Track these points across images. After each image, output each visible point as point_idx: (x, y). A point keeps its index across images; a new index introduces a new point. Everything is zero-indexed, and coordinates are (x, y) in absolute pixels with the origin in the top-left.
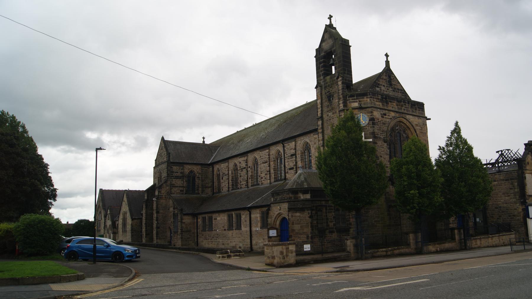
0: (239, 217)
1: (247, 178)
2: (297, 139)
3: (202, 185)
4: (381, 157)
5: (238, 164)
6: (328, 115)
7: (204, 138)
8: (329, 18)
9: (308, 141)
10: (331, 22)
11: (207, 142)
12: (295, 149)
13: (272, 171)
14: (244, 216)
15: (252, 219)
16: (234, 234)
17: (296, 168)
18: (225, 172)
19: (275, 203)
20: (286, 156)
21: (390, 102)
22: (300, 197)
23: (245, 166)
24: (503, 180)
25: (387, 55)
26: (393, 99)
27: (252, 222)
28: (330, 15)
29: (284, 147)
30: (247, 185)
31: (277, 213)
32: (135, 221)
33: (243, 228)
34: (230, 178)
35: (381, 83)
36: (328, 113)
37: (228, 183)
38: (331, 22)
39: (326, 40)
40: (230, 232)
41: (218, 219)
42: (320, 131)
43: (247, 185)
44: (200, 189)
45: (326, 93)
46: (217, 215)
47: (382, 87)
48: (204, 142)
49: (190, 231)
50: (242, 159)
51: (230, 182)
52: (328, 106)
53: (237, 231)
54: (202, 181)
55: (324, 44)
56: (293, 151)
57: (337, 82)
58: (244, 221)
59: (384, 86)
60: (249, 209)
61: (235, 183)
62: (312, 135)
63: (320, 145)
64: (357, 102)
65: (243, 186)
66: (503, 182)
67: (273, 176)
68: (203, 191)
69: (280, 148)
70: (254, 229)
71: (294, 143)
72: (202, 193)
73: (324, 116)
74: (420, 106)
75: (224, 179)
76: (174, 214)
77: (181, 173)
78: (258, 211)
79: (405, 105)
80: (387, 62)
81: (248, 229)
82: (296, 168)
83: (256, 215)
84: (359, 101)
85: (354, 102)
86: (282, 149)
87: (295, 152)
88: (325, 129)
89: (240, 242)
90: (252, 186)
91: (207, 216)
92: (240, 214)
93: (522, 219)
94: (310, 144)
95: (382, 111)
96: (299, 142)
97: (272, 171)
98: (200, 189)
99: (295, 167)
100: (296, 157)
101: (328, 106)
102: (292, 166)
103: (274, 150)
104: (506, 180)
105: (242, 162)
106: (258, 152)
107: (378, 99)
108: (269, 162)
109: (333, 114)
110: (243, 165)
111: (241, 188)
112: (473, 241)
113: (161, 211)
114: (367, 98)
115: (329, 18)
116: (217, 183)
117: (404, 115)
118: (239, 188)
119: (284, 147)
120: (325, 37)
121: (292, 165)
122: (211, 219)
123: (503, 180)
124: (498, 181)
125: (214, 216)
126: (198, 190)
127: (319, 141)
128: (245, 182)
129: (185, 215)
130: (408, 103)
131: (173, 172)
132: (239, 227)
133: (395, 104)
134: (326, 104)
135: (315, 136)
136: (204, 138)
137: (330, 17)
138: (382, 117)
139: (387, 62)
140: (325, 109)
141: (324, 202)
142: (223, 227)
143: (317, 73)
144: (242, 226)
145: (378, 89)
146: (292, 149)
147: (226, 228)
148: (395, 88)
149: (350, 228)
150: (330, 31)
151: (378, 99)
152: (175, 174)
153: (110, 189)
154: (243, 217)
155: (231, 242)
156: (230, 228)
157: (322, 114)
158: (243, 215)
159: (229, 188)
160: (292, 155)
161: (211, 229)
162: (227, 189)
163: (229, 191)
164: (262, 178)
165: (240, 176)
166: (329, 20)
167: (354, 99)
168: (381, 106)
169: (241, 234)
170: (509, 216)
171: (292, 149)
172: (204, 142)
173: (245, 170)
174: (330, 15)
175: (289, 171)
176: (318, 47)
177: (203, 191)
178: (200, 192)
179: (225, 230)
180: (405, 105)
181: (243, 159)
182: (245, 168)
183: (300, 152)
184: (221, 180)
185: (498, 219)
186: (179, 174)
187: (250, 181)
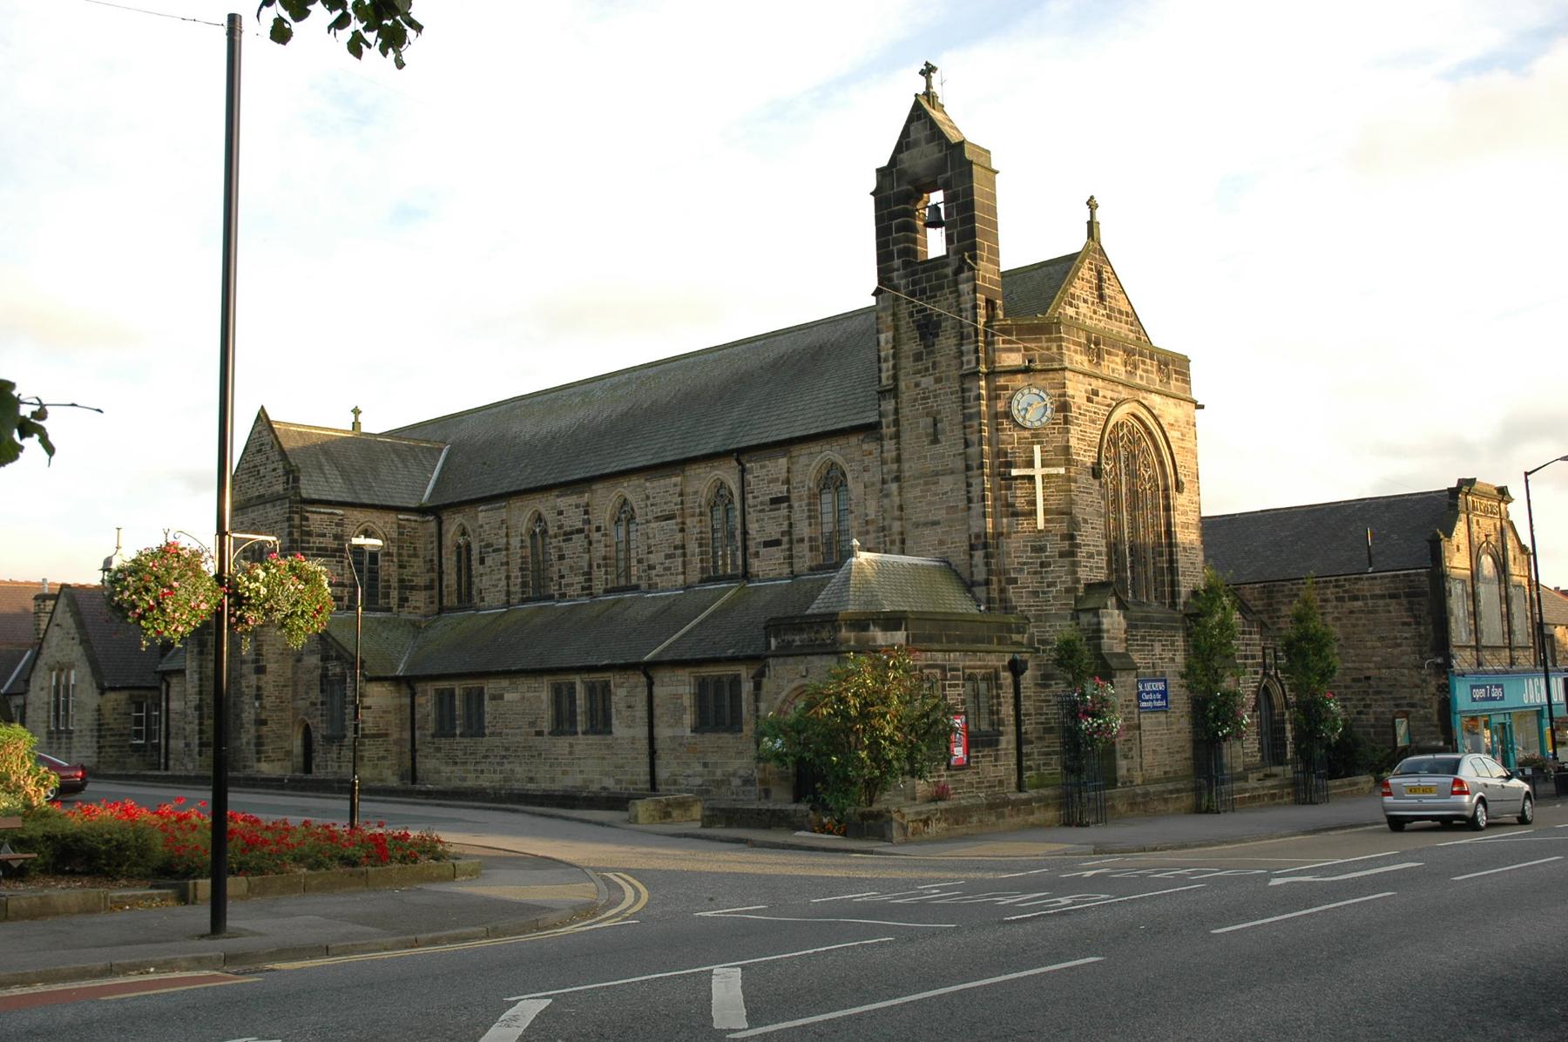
0: (600, 698)
1: (590, 566)
2: (796, 450)
3: (401, 581)
4: (1086, 521)
5: (549, 516)
6: (917, 385)
7: (356, 412)
8: (922, 73)
9: (839, 460)
10: (929, 86)
11: (374, 424)
12: (788, 481)
13: (692, 547)
14: (625, 693)
15: (656, 701)
16: (577, 749)
17: (785, 541)
18: (493, 540)
19: (786, 652)
20: (750, 501)
21: (1109, 353)
22: (874, 640)
23: (580, 525)
24: (1383, 597)
25: (1092, 204)
26: (1116, 343)
27: (657, 712)
28: (927, 64)
29: (743, 471)
30: (587, 589)
31: (795, 684)
32: (112, 696)
33: (619, 729)
34: (516, 562)
35: (1078, 293)
36: (918, 378)
37: (508, 577)
38: (929, 86)
39: (916, 143)
40: (563, 743)
41: (508, 696)
42: (888, 431)
43: (587, 589)
44: (394, 594)
45: (911, 314)
46: (505, 683)
47: (1081, 304)
48: (356, 425)
49: (386, 735)
50: (566, 502)
51: (515, 573)
52: (918, 357)
53: (592, 738)
54: (401, 567)
55: (904, 156)
56: (779, 490)
57: (956, 283)
58: (622, 706)
59: (1085, 301)
60: (648, 669)
61: (537, 583)
62: (854, 440)
63: (888, 477)
64: (1018, 350)
65: (570, 592)
66: (1381, 602)
67: (696, 562)
68: (403, 600)
69: (727, 473)
70: (663, 732)
71: (783, 461)
72: (400, 606)
73: (902, 385)
74: (1174, 366)
75: (489, 561)
76: (324, 676)
77: (336, 537)
78: (685, 675)
79: (1144, 363)
80: (1092, 226)
81: (641, 732)
82: (791, 542)
83: (678, 688)
84: (1026, 349)
85: (1011, 350)
86: (737, 477)
87: (788, 491)
88: (904, 424)
89: (607, 774)
90: (607, 592)
91: (459, 687)
92: (606, 685)
93: (1435, 718)
94: (846, 467)
95: (1087, 380)
96: (803, 460)
97: (692, 547)
98: (394, 594)
99: (785, 539)
100: (790, 507)
101: (918, 357)
102: (778, 536)
103: (701, 481)
104: (1392, 596)
105: (571, 512)
106: (635, 481)
107: (1079, 344)
108: (683, 516)
109: (938, 380)
110: (574, 520)
111: (563, 596)
112: (231, 825)
113: (271, 667)
114: (1049, 340)
115: (922, 73)
116: (454, 576)
117: (1141, 395)
118: (551, 597)
119: (743, 471)
120: (913, 136)
121: (773, 531)
122: (475, 700)
123: (1383, 597)
124: (1364, 598)
125: (490, 686)
126: (387, 596)
127: (883, 462)
128: (582, 579)
129: (370, 680)
130: (1152, 358)
131: (309, 534)
132: (601, 723)
133: (1118, 360)
134: (910, 346)
135: (865, 447)
136: (356, 412)
137: (928, 71)
138: (1089, 400)
139: (1092, 226)
140: (907, 364)
141: (939, 655)
142: (532, 724)
143: (881, 246)
144: (615, 722)
145: (1070, 311)
146: (776, 480)
147: (546, 726)
148: (1111, 309)
149: (1001, 734)
150: (921, 118)
151: (1079, 344)
152: (316, 542)
153: (83, 582)
154: (619, 695)
155: (565, 773)
156: (563, 723)
157: (895, 378)
158: (621, 686)
159: (508, 593)
160: (776, 501)
161: (476, 728)
162: (504, 598)
163: (508, 603)
164: (651, 567)
165: (561, 557)
166: (923, 79)
167: (1010, 342)
168: (1086, 367)
169: (609, 747)
170: (1397, 706)
171: (776, 480)
172: (356, 425)
173: (578, 540)
174: (927, 64)
175: (763, 551)
176: (884, 162)
177: (403, 600)
178: (394, 602)
179: (539, 733)
180: (1144, 363)
181: (573, 499)
182: (580, 531)
183: (805, 492)
184: (475, 564)
185: (1359, 713)
186: (329, 542)
187: (599, 574)
